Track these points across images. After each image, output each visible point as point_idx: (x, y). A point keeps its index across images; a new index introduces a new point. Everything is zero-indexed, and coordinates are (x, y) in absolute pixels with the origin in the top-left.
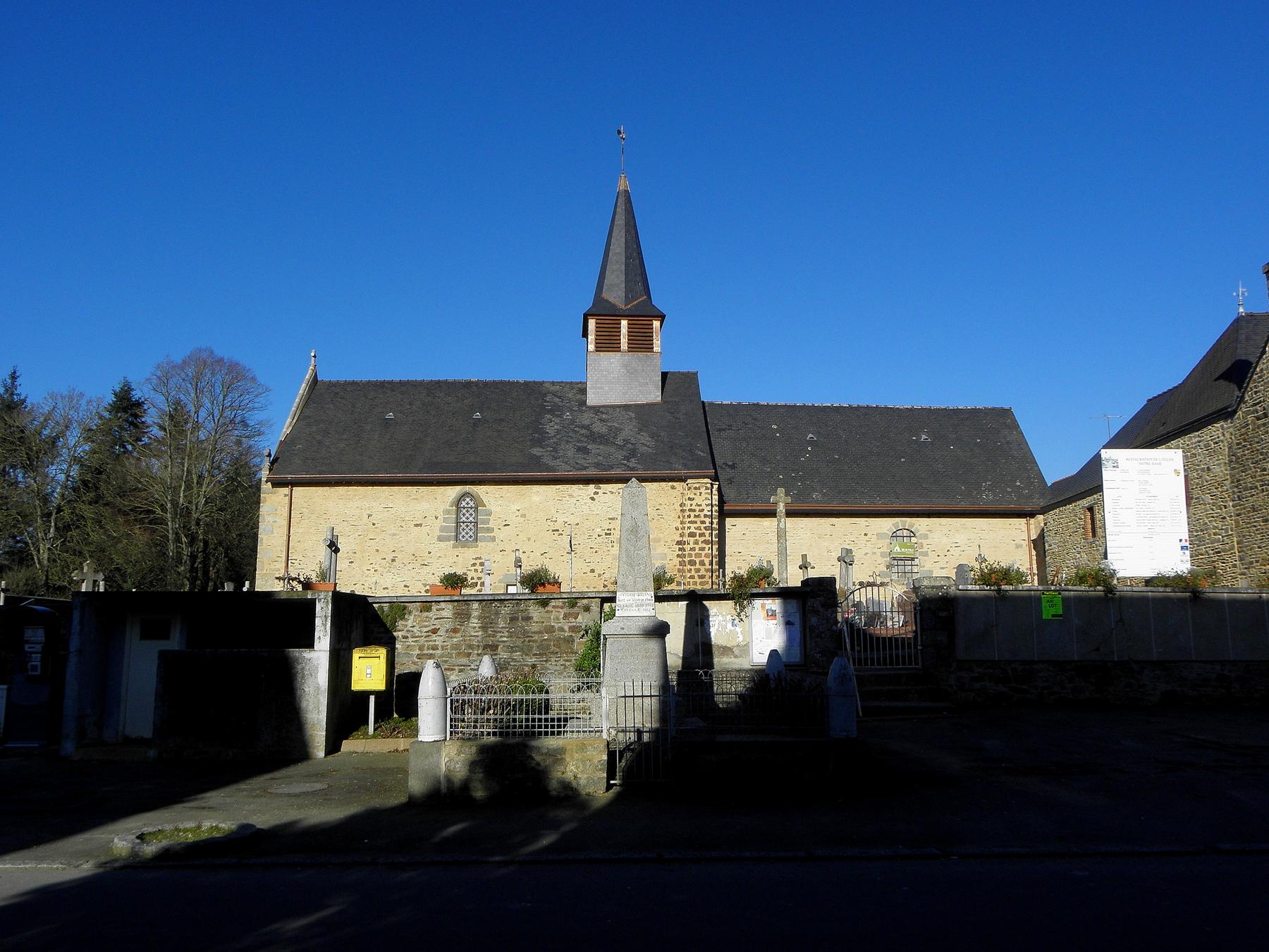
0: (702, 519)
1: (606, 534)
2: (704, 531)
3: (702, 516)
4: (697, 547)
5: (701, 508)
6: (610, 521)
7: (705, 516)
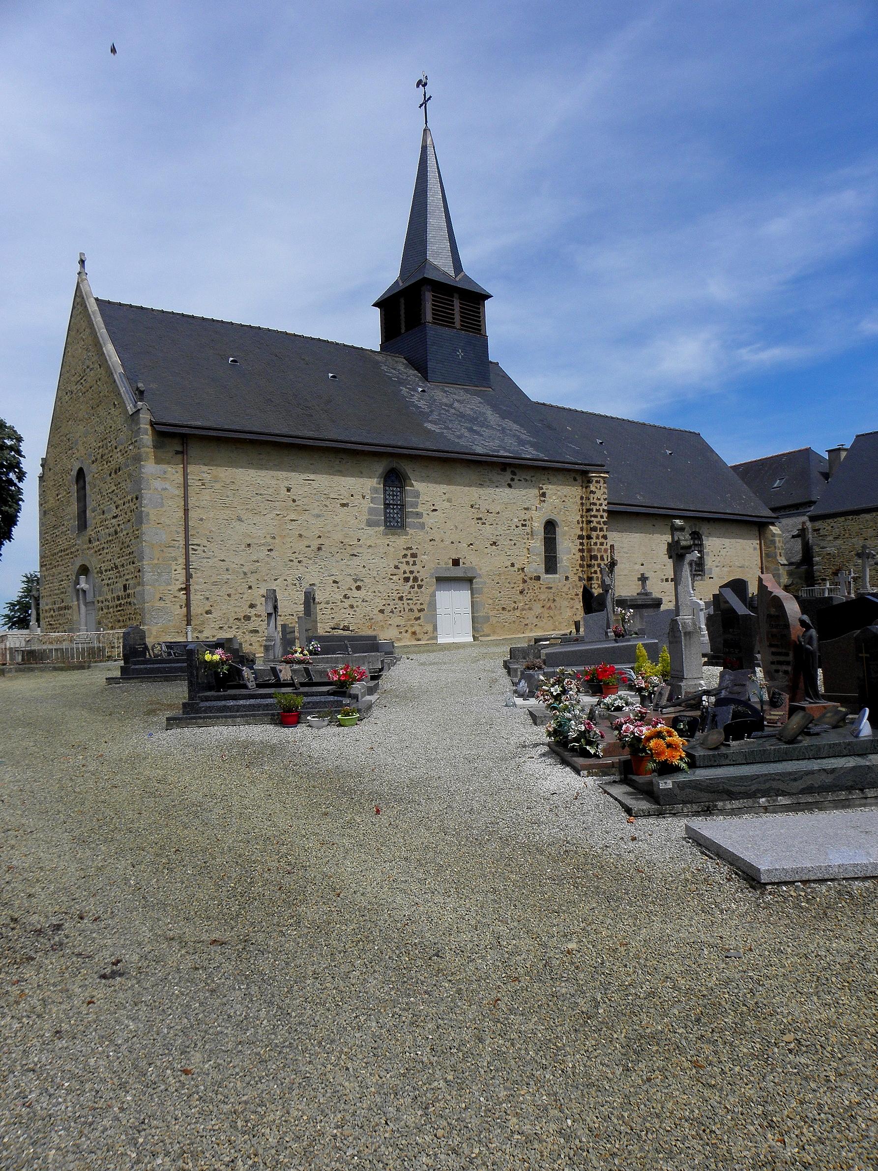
0: (601, 513)
1: (523, 525)
2: (602, 525)
3: (601, 510)
4: (598, 541)
5: (600, 502)
6: (526, 512)
7: (604, 511)
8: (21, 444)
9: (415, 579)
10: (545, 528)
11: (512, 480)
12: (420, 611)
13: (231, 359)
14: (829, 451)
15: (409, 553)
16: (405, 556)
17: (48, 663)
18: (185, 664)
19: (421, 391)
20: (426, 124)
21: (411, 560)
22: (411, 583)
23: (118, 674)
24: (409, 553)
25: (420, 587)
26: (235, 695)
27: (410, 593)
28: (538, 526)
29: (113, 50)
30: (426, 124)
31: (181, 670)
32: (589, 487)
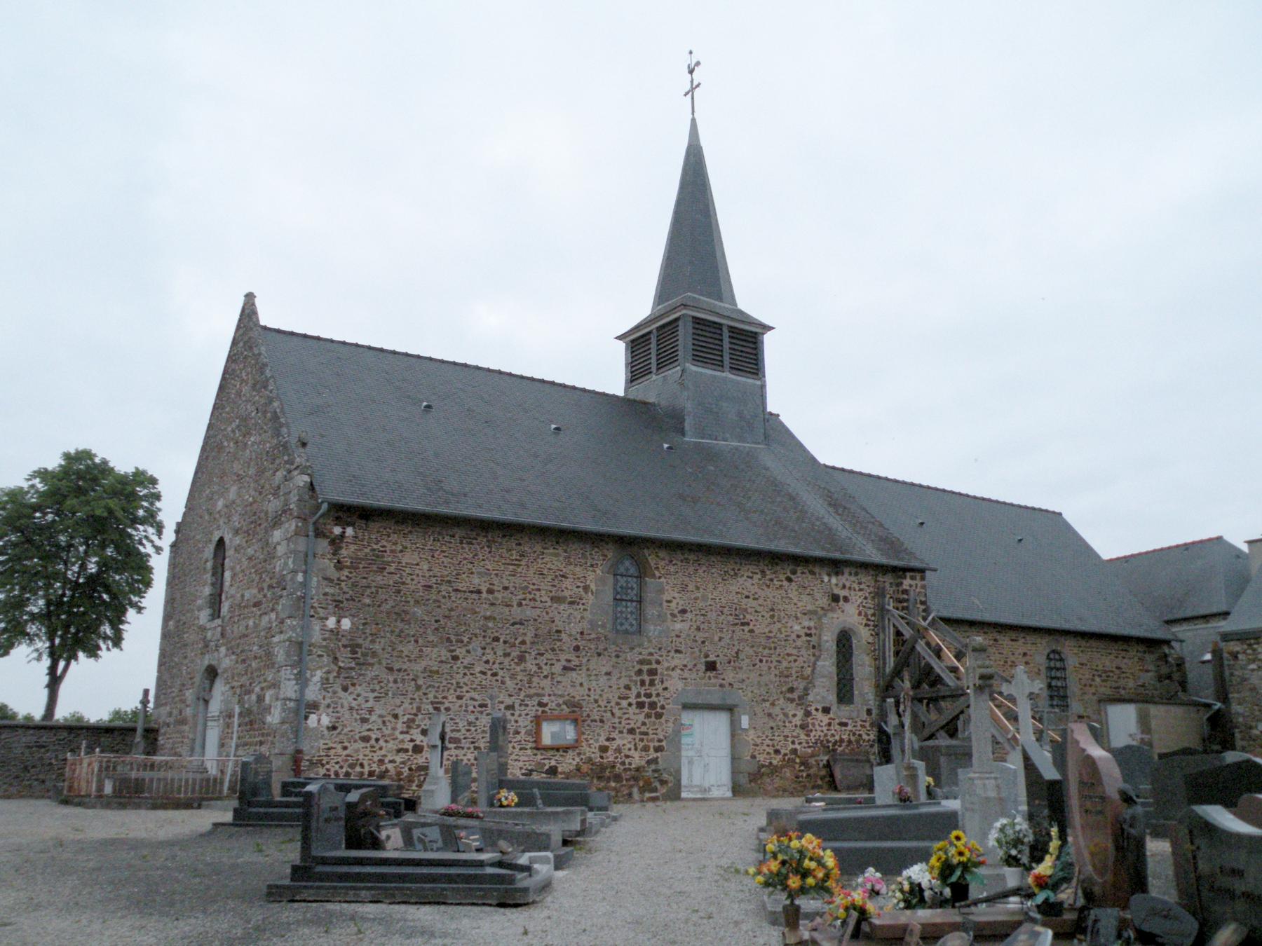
1: (807, 635)
8: (158, 504)
9: (653, 705)
10: (839, 642)
11: (794, 573)
12: (658, 749)
13: (425, 404)
14: (1250, 543)
15: (645, 668)
16: (640, 672)
17: (146, 798)
18: (1152, 809)
19: (668, 448)
20: (693, 114)
21: (647, 678)
22: (646, 710)
23: (228, 817)
24: (645, 668)
25: (659, 716)
26: (362, 859)
27: (644, 724)
28: (829, 639)
29: (691, 53)
30: (693, 114)
31: (292, 818)
32: (902, 583)
